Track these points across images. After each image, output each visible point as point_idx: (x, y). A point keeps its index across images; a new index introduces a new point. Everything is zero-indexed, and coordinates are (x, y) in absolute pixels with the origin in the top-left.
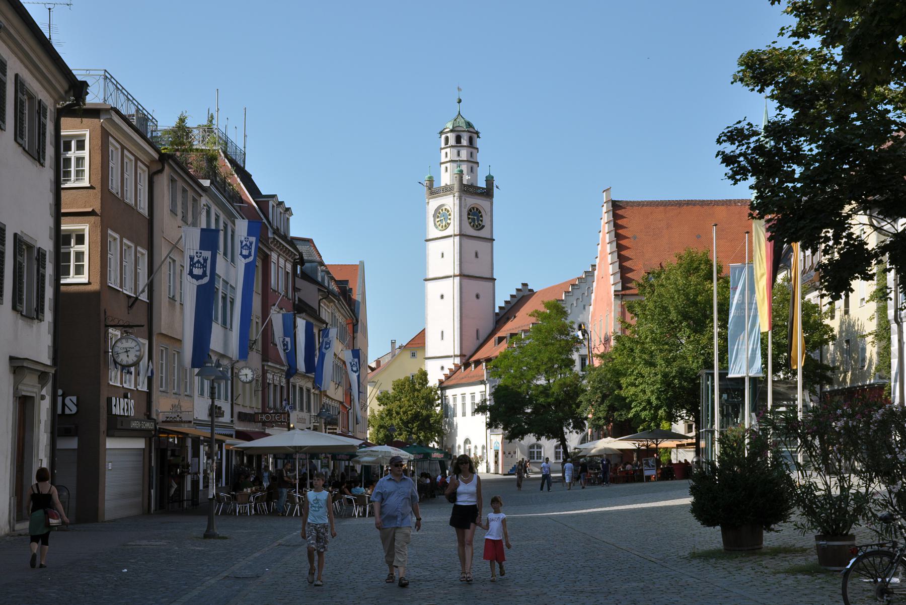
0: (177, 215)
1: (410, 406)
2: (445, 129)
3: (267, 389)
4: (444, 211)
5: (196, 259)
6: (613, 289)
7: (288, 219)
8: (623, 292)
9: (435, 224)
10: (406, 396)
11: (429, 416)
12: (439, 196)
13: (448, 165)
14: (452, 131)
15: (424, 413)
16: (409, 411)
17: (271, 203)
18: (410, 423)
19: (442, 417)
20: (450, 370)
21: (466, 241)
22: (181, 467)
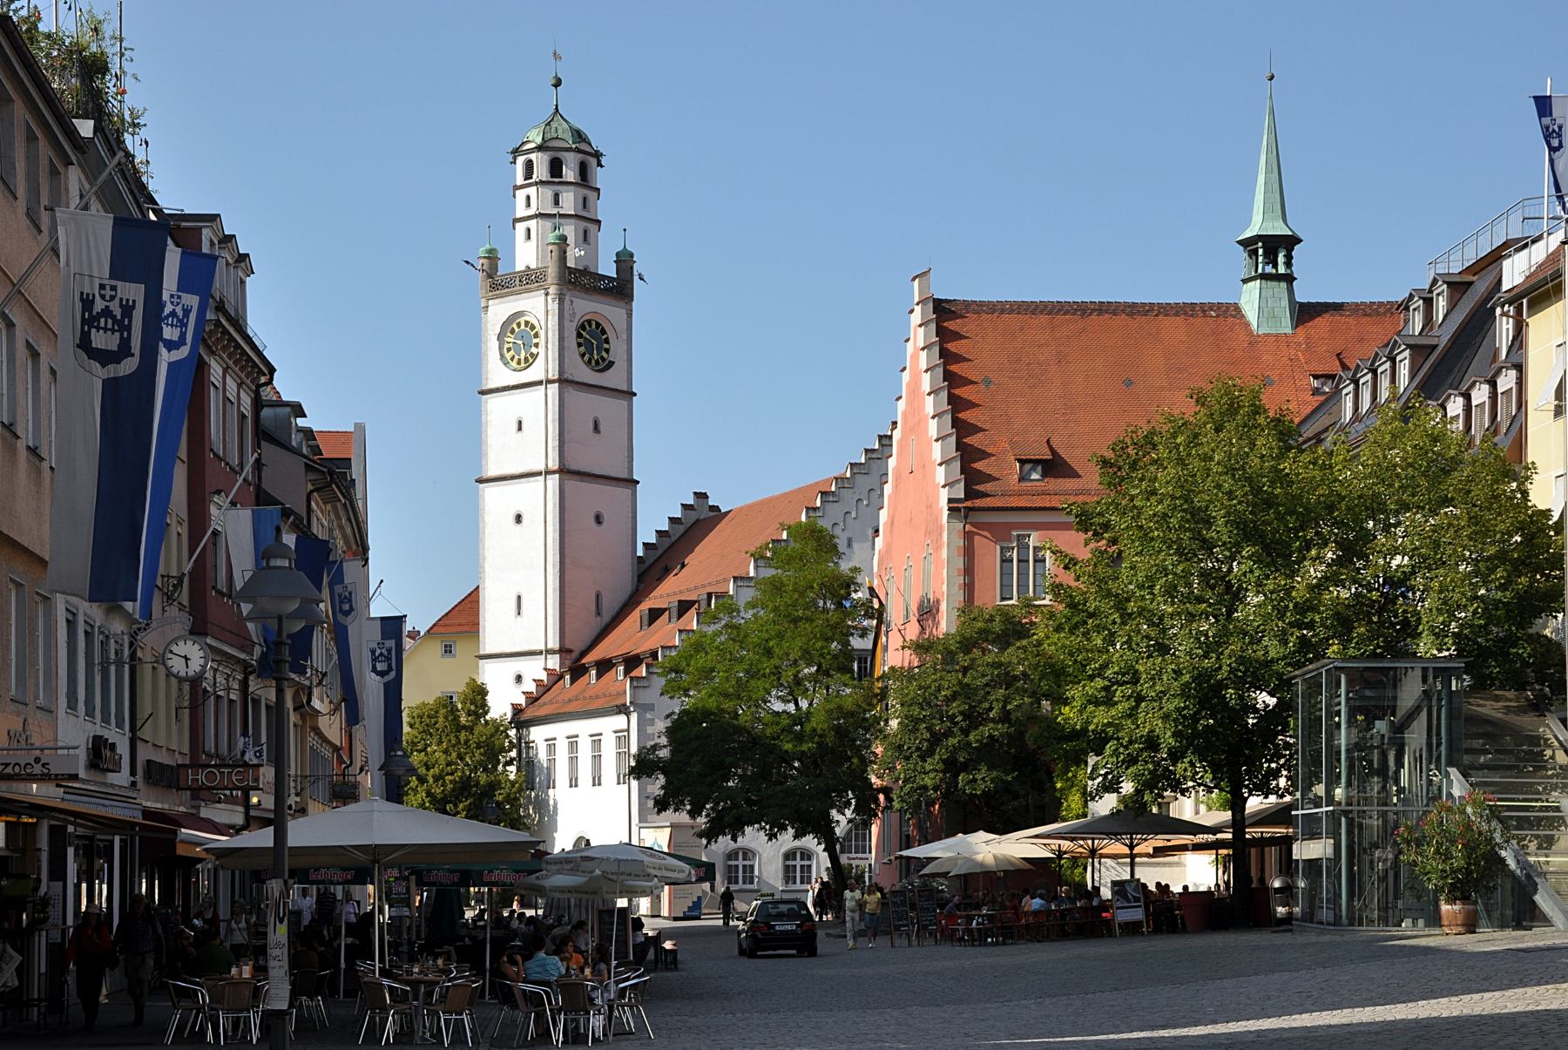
0: (16, 198)
1: (449, 764)
2: (523, 143)
3: (200, 708)
4: (523, 327)
5: (99, 305)
6: (944, 495)
7: (243, 282)
8: (968, 504)
9: (502, 356)
10: (440, 742)
11: (493, 786)
12: (512, 294)
13: (532, 224)
14: (540, 148)
15: (483, 778)
16: (448, 774)
17: (206, 234)
18: (450, 802)
19: (520, 790)
20: (538, 682)
21: (574, 395)
22: (30, 906)
